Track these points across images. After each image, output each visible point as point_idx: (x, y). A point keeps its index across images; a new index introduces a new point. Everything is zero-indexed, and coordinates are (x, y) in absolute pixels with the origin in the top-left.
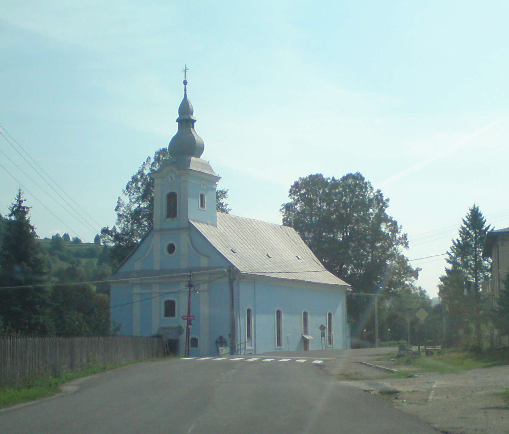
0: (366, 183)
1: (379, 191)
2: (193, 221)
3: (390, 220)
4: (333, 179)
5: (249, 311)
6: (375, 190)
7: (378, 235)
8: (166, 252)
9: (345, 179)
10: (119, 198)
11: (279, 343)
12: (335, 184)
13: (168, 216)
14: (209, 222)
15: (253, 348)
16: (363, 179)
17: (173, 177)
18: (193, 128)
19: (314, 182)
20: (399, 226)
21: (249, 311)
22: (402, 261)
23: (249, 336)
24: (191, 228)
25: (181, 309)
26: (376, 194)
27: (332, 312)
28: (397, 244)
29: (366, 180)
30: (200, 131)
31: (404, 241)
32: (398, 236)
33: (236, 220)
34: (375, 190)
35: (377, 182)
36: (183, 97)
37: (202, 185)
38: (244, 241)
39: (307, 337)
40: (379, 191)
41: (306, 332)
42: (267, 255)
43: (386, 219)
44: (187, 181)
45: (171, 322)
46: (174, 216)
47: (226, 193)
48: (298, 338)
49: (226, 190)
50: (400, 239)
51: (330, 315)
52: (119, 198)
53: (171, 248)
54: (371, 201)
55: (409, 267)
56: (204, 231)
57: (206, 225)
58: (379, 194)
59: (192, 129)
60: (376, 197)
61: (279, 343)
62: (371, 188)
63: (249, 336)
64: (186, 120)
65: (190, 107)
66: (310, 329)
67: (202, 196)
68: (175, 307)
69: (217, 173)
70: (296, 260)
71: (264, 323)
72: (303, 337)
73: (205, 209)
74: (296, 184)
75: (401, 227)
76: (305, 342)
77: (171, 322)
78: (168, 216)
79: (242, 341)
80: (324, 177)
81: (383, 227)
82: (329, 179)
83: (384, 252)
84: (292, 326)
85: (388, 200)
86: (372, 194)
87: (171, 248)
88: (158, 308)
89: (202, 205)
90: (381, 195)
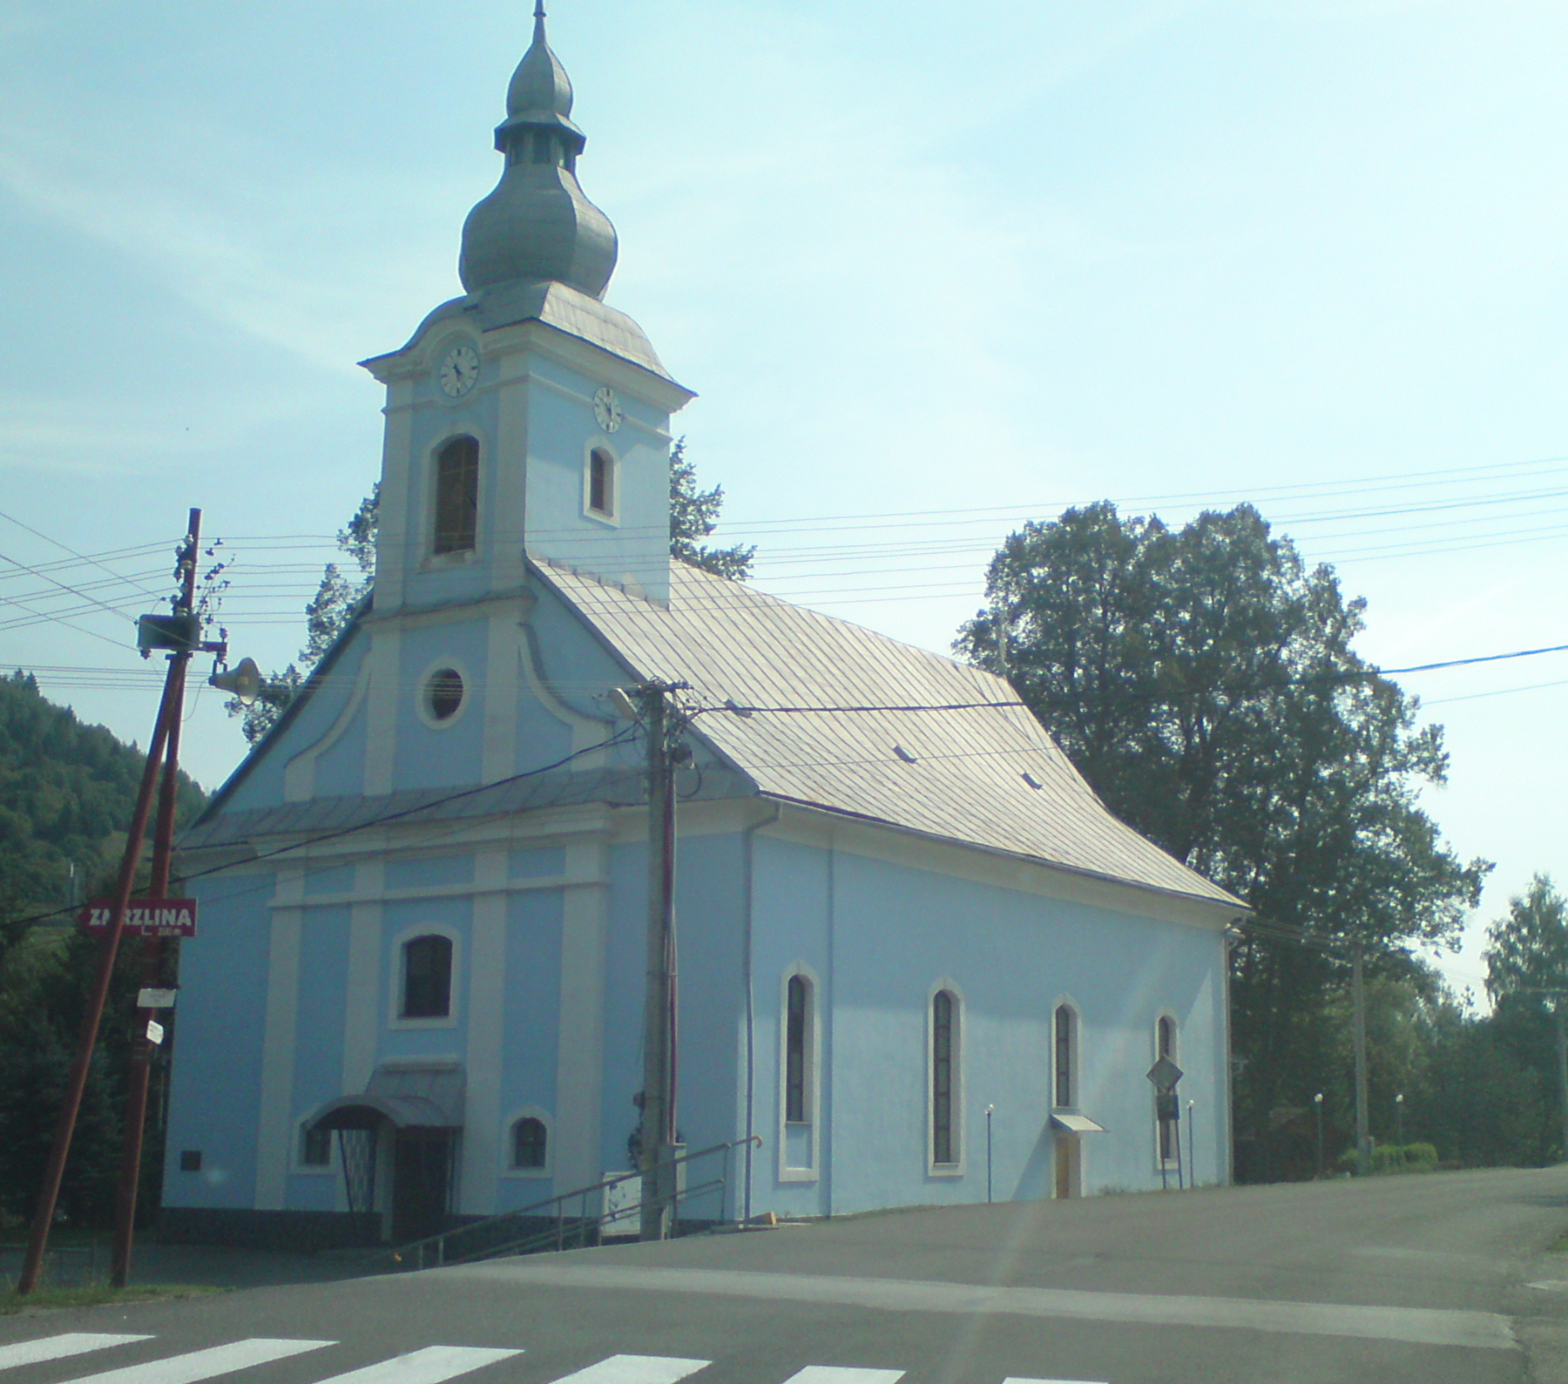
0: (1274, 546)
1: (1324, 572)
2: (551, 563)
3: (1373, 676)
4: (1156, 524)
5: (798, 987)
6: (1309, 569)
7: (1320, 734)
8: (424, 714)
9: (1194, 534)
10: (330, 568)
11: (944, 1150)
12: (1163, 547)
13: (442, 547)
14: (627, 579)
15: (815, 1173)
16: (1261, 528)
17: (464, 369)
18: (570, 167)
19: (1083, 539)
20: (1407, 700)
21: (798, 987)
22: (1416, 830)
23: (797, 1110)
24: (534, 591)
25: (477, 978)
26: (1313, 582)
27: (1172, 1014)
28: (1401, 766)
29: (1274, 535)
30: (598, 185)
31: (1430, 756)
32: (1402, 734)
33: (764, 607)
34: (1309, 569)
35: (1315, 537)
36: (529, 42)
37: (601, 410)
38: (795, 683)
39: (1073, 1123)
40: (1324, 572)
41: (1065, 1100)
42: (898, 751)
43: (1357, 675)
44: (524, 379)
45: (424, 1042)
46: (468, 542)
47: (744, 560)
48: (1032, 1129)
49: (744, 551)
50: (1412, 747)
51: (1166, 1026)
52: (330, 568)
53: (445, 698)
54: (1294, 612)
55: (1441, 860)
56: (598, 608)
57: (616, 595)
58: (1326, 593)
59: (563, 174)
60: (1316, 593)
61: (944, 1150)
62: (1295, 560)
63: (797, 1110)
64: (537, 132)
65: (559, 81)
66: (1087, 1087)
67: (600, 464)
68: (449, 966)
69: (673, 365)
70: (1019, 788)
71: (874, 1050)
72: (1055, 1125)
73: (615, 521)
74: (1015, 543)
75: (1416, 702)
76: (1060, 1140)
77: (424, 1042)
78: (442, 547)
79: (761, 1128)
80: (1122, 516)
81: (1343, 702)
82: (1139, 521)
83: (1346, 795)
84: (1002, 1059)
85: (1361, 603)
86: (1298, 584)
87: (445, 698)
88: (376, 977)
89: (599, 499)
90: (1333, 585)
